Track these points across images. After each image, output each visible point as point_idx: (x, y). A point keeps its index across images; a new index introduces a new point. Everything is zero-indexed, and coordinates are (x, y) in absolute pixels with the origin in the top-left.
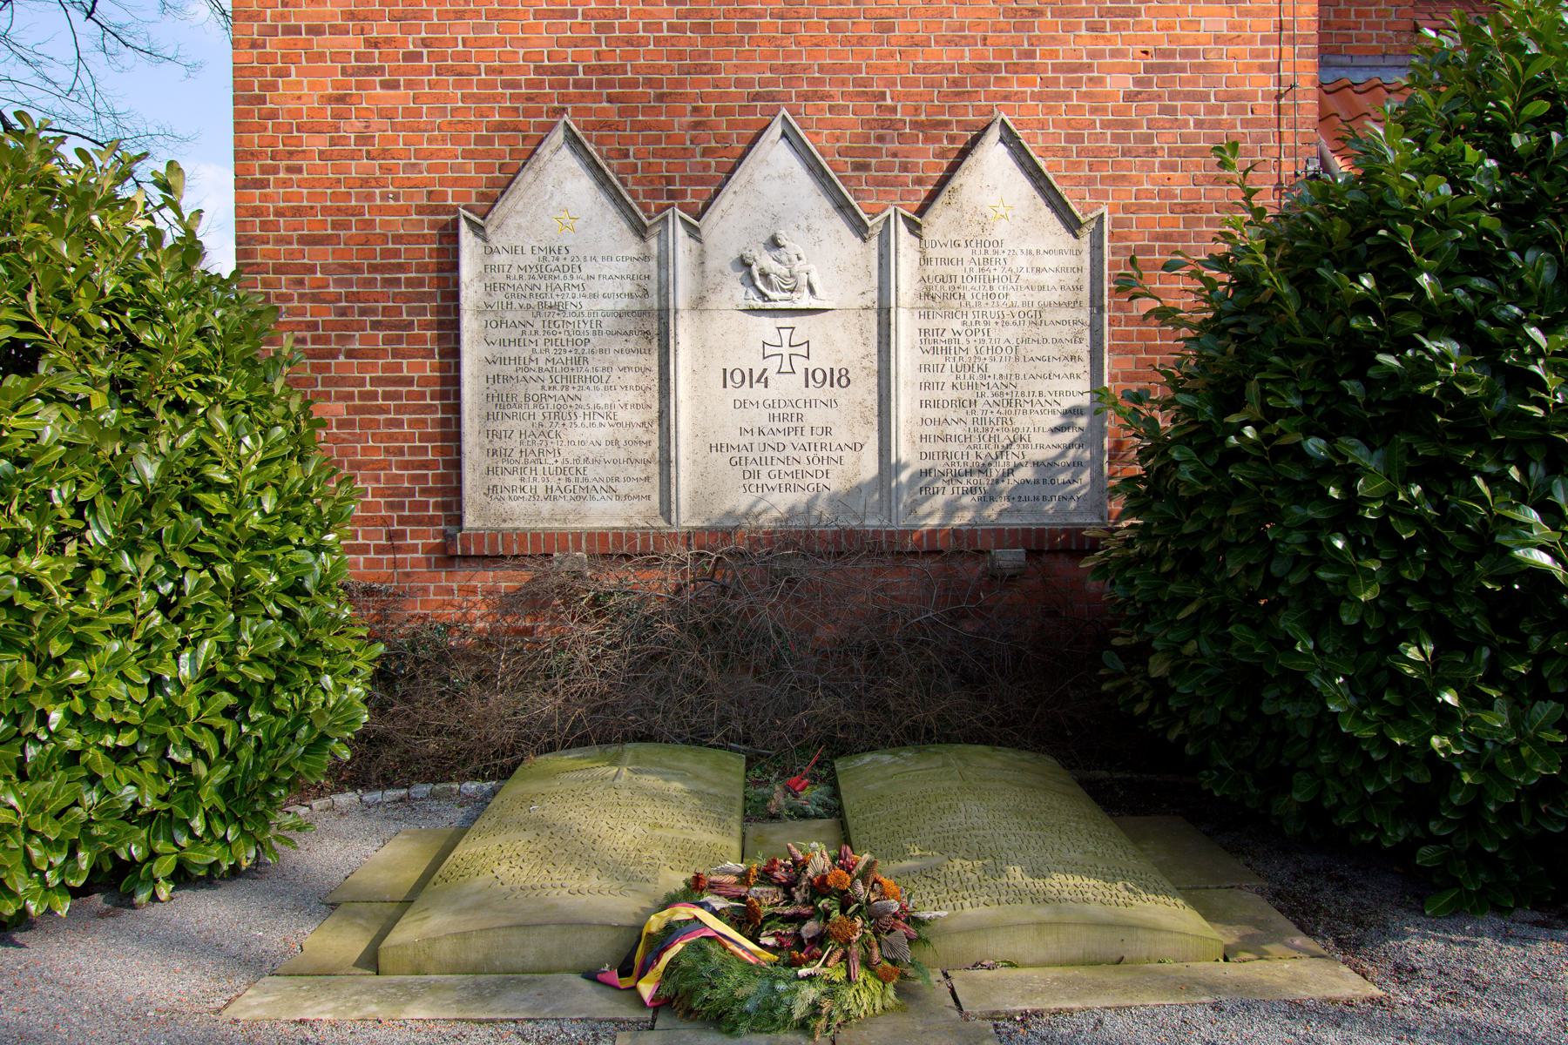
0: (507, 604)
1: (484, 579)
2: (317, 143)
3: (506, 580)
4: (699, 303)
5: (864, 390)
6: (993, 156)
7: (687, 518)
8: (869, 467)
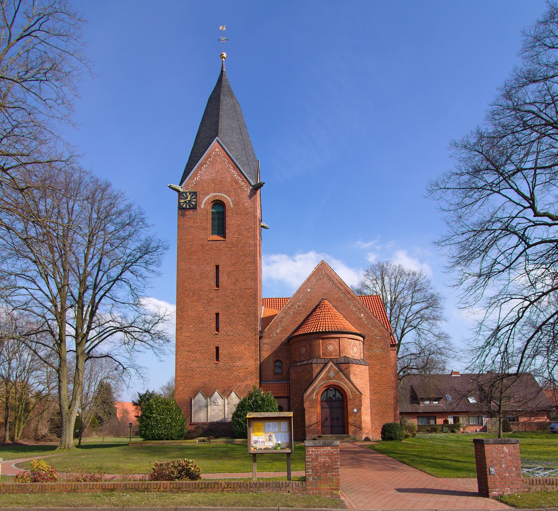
0: (195, 428)
1: (193, 426)
2: (181, 393)
3: (195, 426)
4: (210, 405)
5: (223, 411)
6: (233, 393)
7: (209, 421)
8: (223, 417)
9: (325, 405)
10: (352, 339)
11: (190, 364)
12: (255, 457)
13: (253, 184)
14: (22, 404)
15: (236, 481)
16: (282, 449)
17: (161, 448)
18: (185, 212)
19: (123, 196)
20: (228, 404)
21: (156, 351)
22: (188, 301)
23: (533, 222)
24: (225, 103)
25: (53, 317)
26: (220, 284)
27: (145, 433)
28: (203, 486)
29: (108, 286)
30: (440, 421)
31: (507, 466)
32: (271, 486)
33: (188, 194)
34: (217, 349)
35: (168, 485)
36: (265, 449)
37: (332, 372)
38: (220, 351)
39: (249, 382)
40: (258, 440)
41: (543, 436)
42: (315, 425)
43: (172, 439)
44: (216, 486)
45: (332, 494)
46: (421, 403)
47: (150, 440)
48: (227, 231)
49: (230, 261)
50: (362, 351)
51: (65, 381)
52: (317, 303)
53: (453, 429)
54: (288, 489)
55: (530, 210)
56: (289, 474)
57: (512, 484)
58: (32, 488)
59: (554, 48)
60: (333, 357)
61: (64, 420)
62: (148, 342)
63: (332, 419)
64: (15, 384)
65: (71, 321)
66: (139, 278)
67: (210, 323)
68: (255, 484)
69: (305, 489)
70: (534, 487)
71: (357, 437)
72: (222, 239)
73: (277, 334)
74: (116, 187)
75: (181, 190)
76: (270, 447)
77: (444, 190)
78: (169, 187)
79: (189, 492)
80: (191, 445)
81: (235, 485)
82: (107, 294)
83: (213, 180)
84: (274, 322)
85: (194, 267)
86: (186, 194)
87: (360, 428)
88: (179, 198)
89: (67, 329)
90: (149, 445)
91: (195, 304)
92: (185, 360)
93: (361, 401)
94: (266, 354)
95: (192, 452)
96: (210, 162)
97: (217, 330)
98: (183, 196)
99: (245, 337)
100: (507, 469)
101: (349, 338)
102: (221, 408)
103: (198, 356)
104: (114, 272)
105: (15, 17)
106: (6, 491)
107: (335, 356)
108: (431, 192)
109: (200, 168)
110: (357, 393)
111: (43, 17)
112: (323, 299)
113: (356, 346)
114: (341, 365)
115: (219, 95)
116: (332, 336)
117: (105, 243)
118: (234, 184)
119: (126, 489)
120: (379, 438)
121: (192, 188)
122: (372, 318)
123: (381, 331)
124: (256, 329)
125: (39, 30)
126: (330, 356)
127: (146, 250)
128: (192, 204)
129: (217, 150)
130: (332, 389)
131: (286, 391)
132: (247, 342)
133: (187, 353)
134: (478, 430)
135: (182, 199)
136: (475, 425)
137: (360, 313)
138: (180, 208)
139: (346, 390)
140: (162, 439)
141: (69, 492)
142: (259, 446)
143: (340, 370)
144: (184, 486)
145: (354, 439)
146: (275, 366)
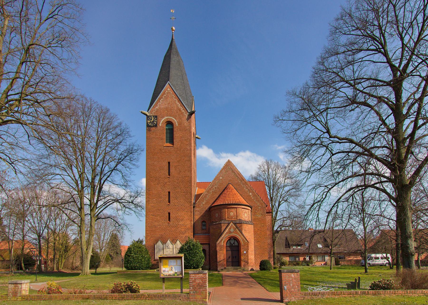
6: (178, 241)
9: (229, 249)
10: (244, 208)
11: (154, 223)
12: (164, 280)
13: (189, 112)
14: (63, 247)
15: (153, 294)
16: (177, 275)
17: (135, 275)
18: (151, 128)
19: (116, 117)
20: (175, 248)
21: (137, 214)
22: (153, 184)
23: (332, 141)
24: (174, 59)
25: (76, 193)
26: (170, 174)
27: (127, 266)
28: (136, 297)
29: (109, 174)
30: (301, 259)
31: (293, 285)
32: (171, 296)
33: (152, 117)
34: (169, 213)
35: (117, 296)
36: (169, 275)
37: (232, 229)
38: (171, 215)
39: (187, 235)
40: (165, 270)
41: (356, 268)
42: (223, 261)
43: (142, 269)
44: (142, 297)
45: (203, 301)
46: (291, 247)
47: (130, 270)
48: (174, 141)
49: (176, 159)
50: (250, 216)
51: (84, 233)
52: (226, 186)
53: (307, 264)
54: (180, 298)
55: (327, 134)
56: (182, 290)
57: (296, 295)
58: (44, 297)
59: (345, 34)
60: (233, 220)
61: (84, 257)
62: (133, 209)
63: (233, 257)
64: (58, 235)
65: (87, 196)
66: (127, 169)
67: (165, 198)
68: (163, 295)
69: (189, 298)
70: (307, 297)
71: (246, 269)
72: (172, 145)
73: (203, 205)
74: (112, 111)
75: (148, 114)
76: (172, 274)
77: (282, 121)
78: (141, 112)
79: (128, 300)
80: (152, 273)
81: (152, 296)
82: (108, 179)
83: (167, 109)
84: (202, 197)
85: (155, 163)
86: (151, 117)
87: (247, 263)
88: (147, 120)
89: (85, 201)
90: (128, 273)
91: (156, 186)
92: (151, 221)
93: (248, 246)
94: (197, 217)
95: (150, 277)
96: (165, 97)
97: (169, 202)
98: (149, 118)
99: (185, 206)
100: (293, 287)
101: (242, 208)
102: (171, 250)
103: (158, 218)
104: (113, 164)
105: (43, 6)
106: (31, 299)
107: (234, 219)
108: (275, 122)
109: (159, 101)
110: (246, 241)
111: (60, 6)
112: (229, 184)
113: (246, 213)
114: (237, 224)
115: (170, 54)
116: (233, 206)
117: (107, 146)
118: (178, 111)
119: (95, 298)
120: (258, 268)
121: (154, 113)
122: (256, 196)
123: (261, 204)
124: (191, 202)
125: (57, 15)
126: (231, 219)
127: (130, 152)
128: (155, 124)
129: (169, 89)
130: (232, 239)
131: (208, 240)
132: (186, 210)
133: (152, 216)
134: (323, 264)
135: (149, 120)
136: (321, 261)
137: (250, 192)
138: (148, 126)
139: (239, 239)
140: (137, 269)
141: (64, 300)
142: (166, 273)
143: (237, 227)
144: (126, 296)
145: (244, 269)
146: (202, 225)
